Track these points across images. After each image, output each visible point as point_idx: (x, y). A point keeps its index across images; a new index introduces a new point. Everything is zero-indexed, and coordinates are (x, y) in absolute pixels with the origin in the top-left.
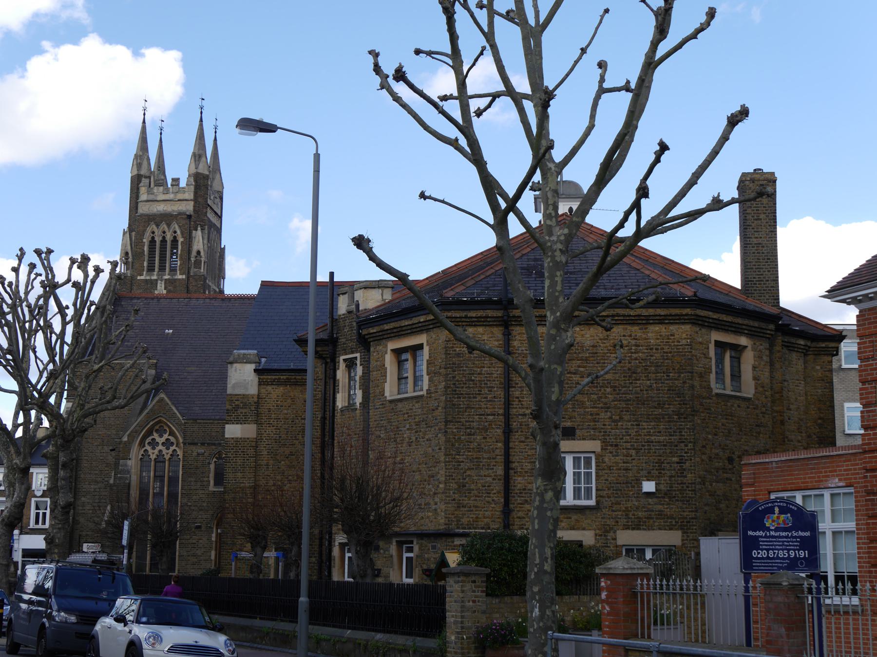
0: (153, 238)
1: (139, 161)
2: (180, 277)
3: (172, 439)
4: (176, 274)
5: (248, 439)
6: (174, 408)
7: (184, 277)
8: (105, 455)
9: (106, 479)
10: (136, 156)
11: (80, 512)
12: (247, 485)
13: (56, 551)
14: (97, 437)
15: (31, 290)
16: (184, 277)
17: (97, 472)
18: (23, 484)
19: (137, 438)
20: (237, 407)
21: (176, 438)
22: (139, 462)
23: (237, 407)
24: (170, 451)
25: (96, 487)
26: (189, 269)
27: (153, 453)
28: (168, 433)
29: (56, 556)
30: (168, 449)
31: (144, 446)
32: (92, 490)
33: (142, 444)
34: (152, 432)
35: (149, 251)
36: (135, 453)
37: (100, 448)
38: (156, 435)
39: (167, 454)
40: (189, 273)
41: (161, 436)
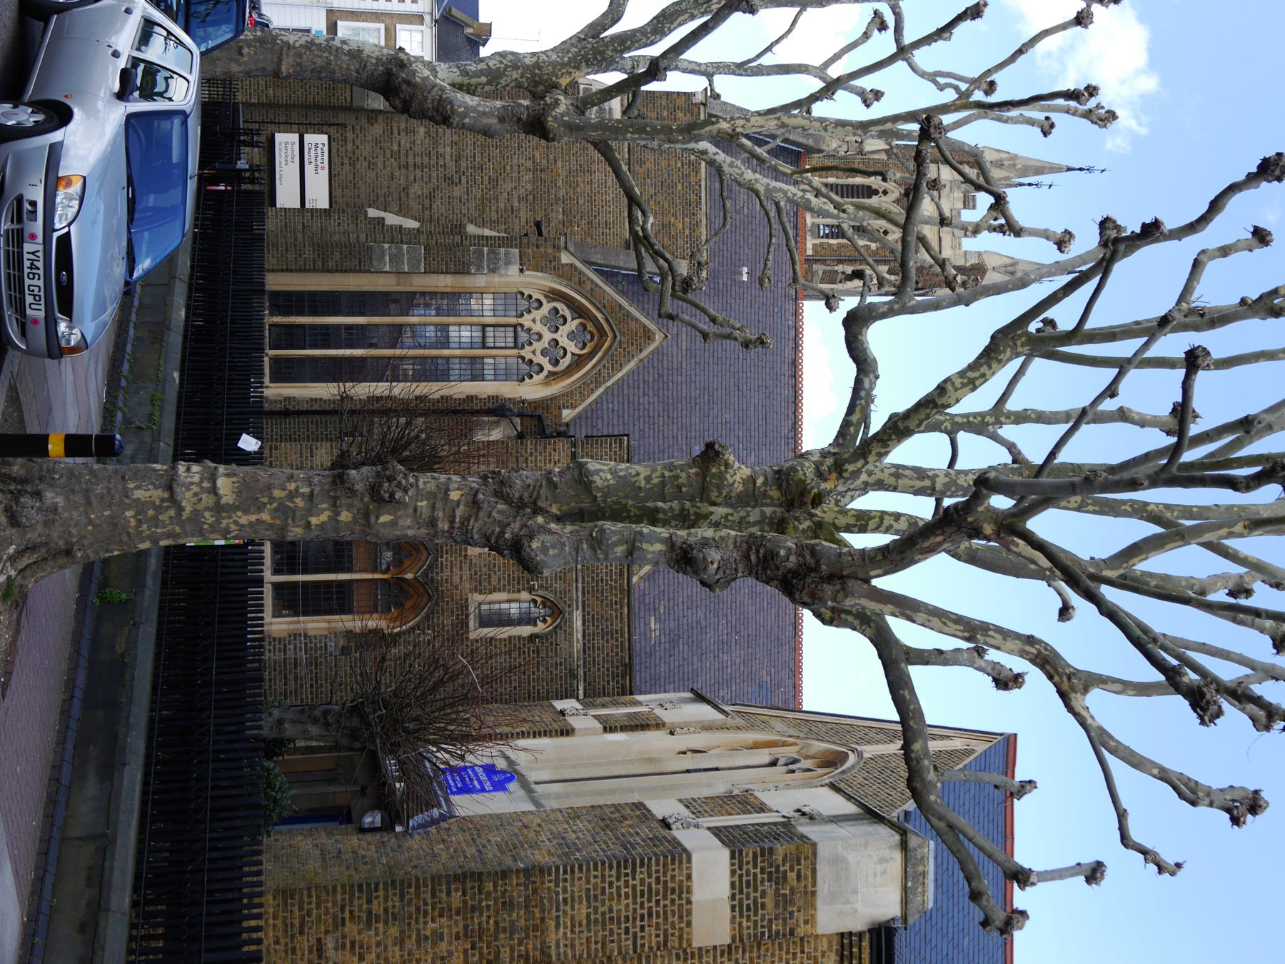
0: (876, 192)
1: (1006, 163)
2: (809, 245)
3: (565, 363)
4: (813, 237)
5: (689, 924)
6: (632, 364)
7: (810, 252)
8: (515, 174)
9: (464, 179)
10: (1014, 157)
11: (395, 125)
12: (552, 938)
13: (345, 516)
14: (551, 156)
15: (935, 83)
16: (810, 252)
17: (478, 156)
18: (502, 120)
19: (567, 286)
20: (778, 878)
21: (569, 371)
22: (515, 290)
23: (778, 878)
24: (539, 359)
25: (448, 157)
26: (823, 262)
27: (534, 321)
28: (578, 352)
29: (324, 517)
30: (544, 352)
31: (550, 300)
32: (441, 150)
33: (554, 295)
34: (580, 317)
35: (853, 186)
36: (536, 282)
37: (529, 164)
38: (572, 325)
39: (534, 352)
40: (817, 261)
41: (571, 336)
